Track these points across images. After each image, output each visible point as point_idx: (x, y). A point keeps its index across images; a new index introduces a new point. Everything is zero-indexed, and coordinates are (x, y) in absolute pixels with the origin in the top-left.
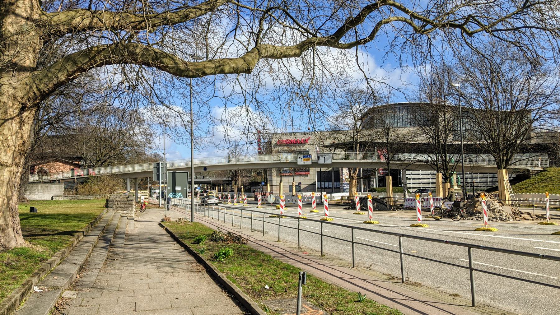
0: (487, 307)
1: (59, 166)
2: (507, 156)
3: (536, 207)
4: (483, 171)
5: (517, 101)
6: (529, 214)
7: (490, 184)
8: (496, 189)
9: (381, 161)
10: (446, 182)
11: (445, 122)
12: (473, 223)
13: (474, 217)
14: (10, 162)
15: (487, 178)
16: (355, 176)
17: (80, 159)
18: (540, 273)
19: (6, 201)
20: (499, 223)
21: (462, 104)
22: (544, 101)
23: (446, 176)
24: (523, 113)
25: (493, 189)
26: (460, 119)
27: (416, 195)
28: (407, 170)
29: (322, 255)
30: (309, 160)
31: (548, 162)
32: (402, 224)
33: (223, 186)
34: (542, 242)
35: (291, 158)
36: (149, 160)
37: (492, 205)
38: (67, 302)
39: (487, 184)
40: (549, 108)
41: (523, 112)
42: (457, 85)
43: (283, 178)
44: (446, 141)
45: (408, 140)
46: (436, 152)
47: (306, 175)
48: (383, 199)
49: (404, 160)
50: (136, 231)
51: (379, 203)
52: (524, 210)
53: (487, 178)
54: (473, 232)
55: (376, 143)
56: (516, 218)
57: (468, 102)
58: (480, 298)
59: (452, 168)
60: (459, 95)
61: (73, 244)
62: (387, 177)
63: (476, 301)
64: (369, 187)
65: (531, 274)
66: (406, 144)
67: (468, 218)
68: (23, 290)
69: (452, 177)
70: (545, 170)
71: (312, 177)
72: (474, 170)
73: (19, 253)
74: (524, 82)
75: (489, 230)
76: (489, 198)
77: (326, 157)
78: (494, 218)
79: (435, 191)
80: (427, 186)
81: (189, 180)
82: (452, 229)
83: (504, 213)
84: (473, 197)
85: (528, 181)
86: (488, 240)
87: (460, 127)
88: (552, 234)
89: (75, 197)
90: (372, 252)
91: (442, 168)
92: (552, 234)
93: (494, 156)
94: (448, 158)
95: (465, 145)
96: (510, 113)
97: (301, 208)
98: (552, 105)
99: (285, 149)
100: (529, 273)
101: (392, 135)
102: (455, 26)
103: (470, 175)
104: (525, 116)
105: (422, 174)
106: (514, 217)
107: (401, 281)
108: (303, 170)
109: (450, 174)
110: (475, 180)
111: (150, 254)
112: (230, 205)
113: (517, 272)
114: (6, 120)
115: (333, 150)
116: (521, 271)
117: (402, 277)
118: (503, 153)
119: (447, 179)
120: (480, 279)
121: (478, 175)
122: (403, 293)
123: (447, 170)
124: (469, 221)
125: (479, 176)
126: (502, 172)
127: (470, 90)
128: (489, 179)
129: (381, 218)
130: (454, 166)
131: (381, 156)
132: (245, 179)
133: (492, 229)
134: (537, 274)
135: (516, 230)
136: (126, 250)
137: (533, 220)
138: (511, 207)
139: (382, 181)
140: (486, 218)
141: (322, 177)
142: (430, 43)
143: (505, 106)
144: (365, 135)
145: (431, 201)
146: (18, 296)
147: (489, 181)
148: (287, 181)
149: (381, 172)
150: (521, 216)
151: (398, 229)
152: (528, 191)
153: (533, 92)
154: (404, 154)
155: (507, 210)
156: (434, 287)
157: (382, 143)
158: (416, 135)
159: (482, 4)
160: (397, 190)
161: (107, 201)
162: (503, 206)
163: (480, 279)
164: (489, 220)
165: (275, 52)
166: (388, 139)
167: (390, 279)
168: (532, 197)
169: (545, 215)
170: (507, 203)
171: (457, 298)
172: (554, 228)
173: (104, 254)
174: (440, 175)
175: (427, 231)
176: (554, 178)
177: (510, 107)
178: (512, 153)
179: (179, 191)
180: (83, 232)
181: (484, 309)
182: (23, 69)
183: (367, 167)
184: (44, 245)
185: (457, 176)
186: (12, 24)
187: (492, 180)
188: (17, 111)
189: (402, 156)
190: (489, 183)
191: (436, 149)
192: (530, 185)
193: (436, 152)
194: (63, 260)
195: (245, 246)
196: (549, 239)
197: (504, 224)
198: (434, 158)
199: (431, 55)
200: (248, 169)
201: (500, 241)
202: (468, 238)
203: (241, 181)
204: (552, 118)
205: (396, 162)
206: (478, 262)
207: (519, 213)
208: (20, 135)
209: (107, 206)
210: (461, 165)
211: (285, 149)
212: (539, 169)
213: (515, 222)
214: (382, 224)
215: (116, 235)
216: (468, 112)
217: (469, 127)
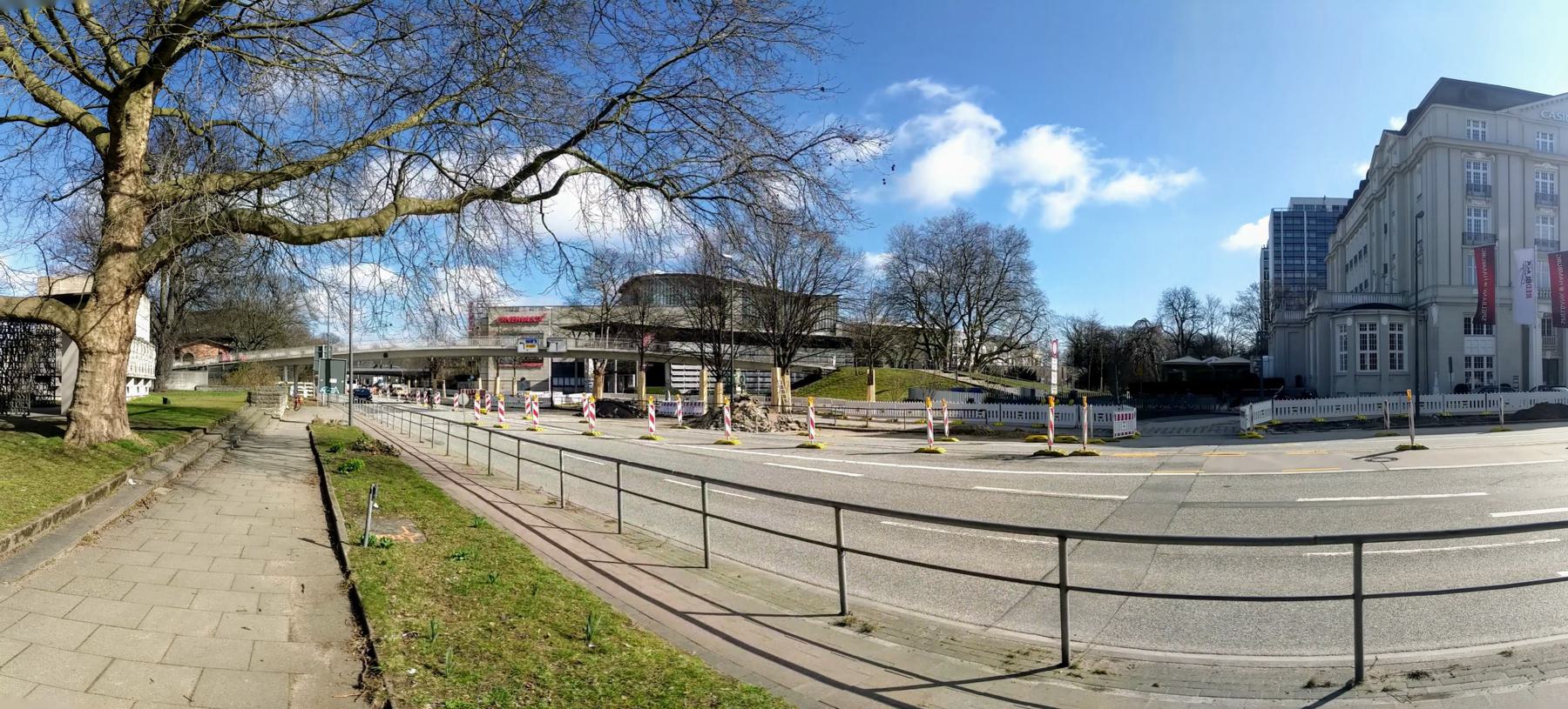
1: (204, 348)
14: (116, 349)
16: (602, 371)
17: (229, 340)
19: (113, 390)
29: (489, 474)
30: (534, 346)
33: (419, 379)
35: (509, 342)
36: (309, 343)
38: (155, 497)
43: (501, 371)
47: (539, 368)
50: (276, 433)
61: (186, 441)
64: (626, 385)
68: (116, 479)
70: (838, 369)
71: (545, 372)
73: (125, 444)
77: (559, 343)
81: (347, 370)
89: (222, 388)
90: (1219, 562)
97: (502, 413)
99: (505, 329)
108: (532, 361)
111: (275, 459)
112: (419, 405)
114: (112, 306)
115: (576, 333)
132: (449, 371)
136: (247, 454)
141: (559, 370)
144: (620, 313)
146: (108, 484)
148: (507, 374)
161: (250, 394)
165: (424, 207)
173: (219, 454)
179: (335, 385)
180: (205, 430)
182: (129, 250)
183: (624, 358)
184: (152, 439)
186: (116, 203)
188: (123, 295)
194: (169, 457)
195: (395, 459)
200: (454, 358)
203: (445, 372)
208: (125, 320)
209: (249, 401)
211: (505, 329)
215: (246, 435)
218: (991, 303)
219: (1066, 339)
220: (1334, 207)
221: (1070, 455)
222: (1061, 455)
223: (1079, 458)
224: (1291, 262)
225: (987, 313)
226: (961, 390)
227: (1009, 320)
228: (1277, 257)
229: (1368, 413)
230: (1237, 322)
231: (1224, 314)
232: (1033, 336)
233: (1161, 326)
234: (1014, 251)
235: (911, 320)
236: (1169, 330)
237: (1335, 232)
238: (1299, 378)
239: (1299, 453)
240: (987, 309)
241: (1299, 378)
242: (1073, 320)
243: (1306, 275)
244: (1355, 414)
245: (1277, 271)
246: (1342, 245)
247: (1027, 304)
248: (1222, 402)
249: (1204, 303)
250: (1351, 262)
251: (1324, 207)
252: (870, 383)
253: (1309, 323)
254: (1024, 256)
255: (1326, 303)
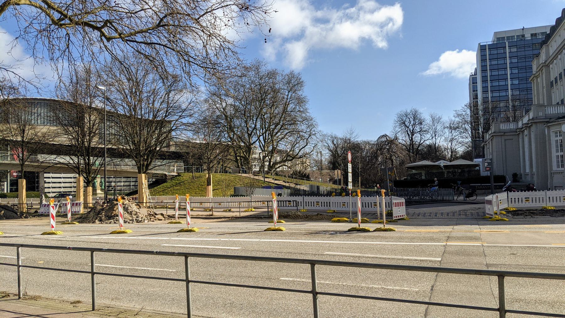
0: (106, 308)
2: (148, 162)
3: (170, 208)
4: (126, 175)
5: (158, 111)
6: (162, 215)
7: (132, 188)
8: (136, 192)
9: (14, 162)
10: (88, 186)
11: (90, 124)
12: (111, 226)
13: (112, 221)
15: (130, 182)
18: (162, 268)
20: (135, 225)
21: (108, 108)
22: (180, 114)
23: (88, 180)
24: (162, 123)
25: (134, 193)
26: (105, 122)
27: (50, 200)
28: (45, 173)
31: (183, 168)
32: (32, 233)
34: (168, 240)
37: (129, 208)
39: (130, 188)
40: (184, 121)
41: (163, 122)
42: (103, 88)
44: (90, 143)
45: (47, 139)
46: (79, 155)
48: (14, 205)
49: (42, 162)
51: (7, 210)
52: (158, 211)
53: (130, 182)
54: (108, 235)
55: (8, 140)
56: (150, 219)
57: (114, 107)
58: (102, 300)
59: (95, 172)
60: (104, 98)
62: (20, 180)
63: (96, 304)
65: (154, 270)
66: (45, 144)
67: (107, 221)
69: (95, 181)
70: (179, 175)
72: (118, 174)
74: (164, 95)
75: (124, 232)
76: (127, 202)
78: (130, 220)
79: (76, 196)
80: (69, 190)
82: (88, 234)
83: (140, 215)
84: (113, 200)
85: (165, 184)
86: (121, 242)
87: (105, 131)
88: (178, 232)
91: (85, 171)
92: (178, 232)
93: (135, 161)
94: (91, 161)
95: (108, 149)
96: (151, 122)
98: (186, 118)
100: (152, 269)
101: (29, 133)
102: (94, 28)
103: (114, 179)
104: (164, 126)
105: (63, 178)
106: (149, 217)
107: (17, 297)
109: (92, 178)
110: (119, 184)
113: (142, 270)
116: (146, 268)
117: (19, 292)
118: (144, 159)
119: (89, 182)
120: (106, 282)
121: (122, 179)
122: (17, 310)
123: (89, 173)
124: (107, 225)
125: (123, 180)
126: (142, 175)
127: (115, 96)
128: (131, 183)
129: (7, 228)
130: (97, 169)
131: (15, 156)
133: (127, 231)
134: (160, 269)
135: (148, 230)
137: (165, 220)
138: (147, 209)
139: (14, 184)
140: (121, 221)
142: (69, 39)
143: (147, 114)
145: (69, 207)
147: (131, 185)
149: (15, 174)
150: (155, 217)
151: (27, 239)
152: (164, 193)
153: (171, 105)
154: (42, 155)
155: (143, 212)
156: (56, 297)
157: (16, 141)
158: (57, 135)
159: (123, 12)
160: (33, 195)
162: (140, 208)
163: (106, 282)
164: (125, 222)
166: (23, 137)
167: (3, 297)
168: (166, 199)
169: (174, 215)
170: (144, 205)
171: (77, 305)
172: (181, 226)
174: (82, 179)
175: (60, 239)
176: (186, 182)
177: (151, 116)
178: (152, 159)
181: (103, 311)
185: (101, 180)
187: (135, 184)
189: (41, 157)
190: (131, 187)
191: (78, 152)
192: (166, 188)
193: (79, 155)
196: (174, 237)
197: (140, 225)
198: (76, 160)
199: (69, 51)
201: (133, 242)
202: (103, 242)
204: (186, 130)
205: (32, 164)
206: (108, 264)
207: (154, 215)
210: (103, 169)
212: (175, 174)
213: (150, 222)
214: (7, 235)
216: (113, 116)
217: (113, 131)
218: (279, 127)
219: (327, 151)
220: (532, 35)
221: (374, 231)
222: (368, 231)
223: (382, 232)
224: (497, 84)
225: (277, 133)
226: (269, 187)
227: (290, 138)
228: (484, 80)
229: (555, 204)
230: (455, 133)
231: (444, 128)
232: (307, 150)
233: (396, 138)
234: (294, 89)
235: (225, 139)
236: (404, 142)
237: (538, 55)
238: (515, 176)
239: (552, 231)
240: (276, 131)
241: (515, 176)
242: (332, 137)
243: (510, 92)
244: (544, 205)
245: (485, 91)
246: (546, 65)
247: (303, 127)
248: (460, 194)
249: (428, 120)
250: (556, 79)
251: (523, 36)
252: (209, 184)
253: (523, 132)
254: (300, 93)
255: (541, 114)
